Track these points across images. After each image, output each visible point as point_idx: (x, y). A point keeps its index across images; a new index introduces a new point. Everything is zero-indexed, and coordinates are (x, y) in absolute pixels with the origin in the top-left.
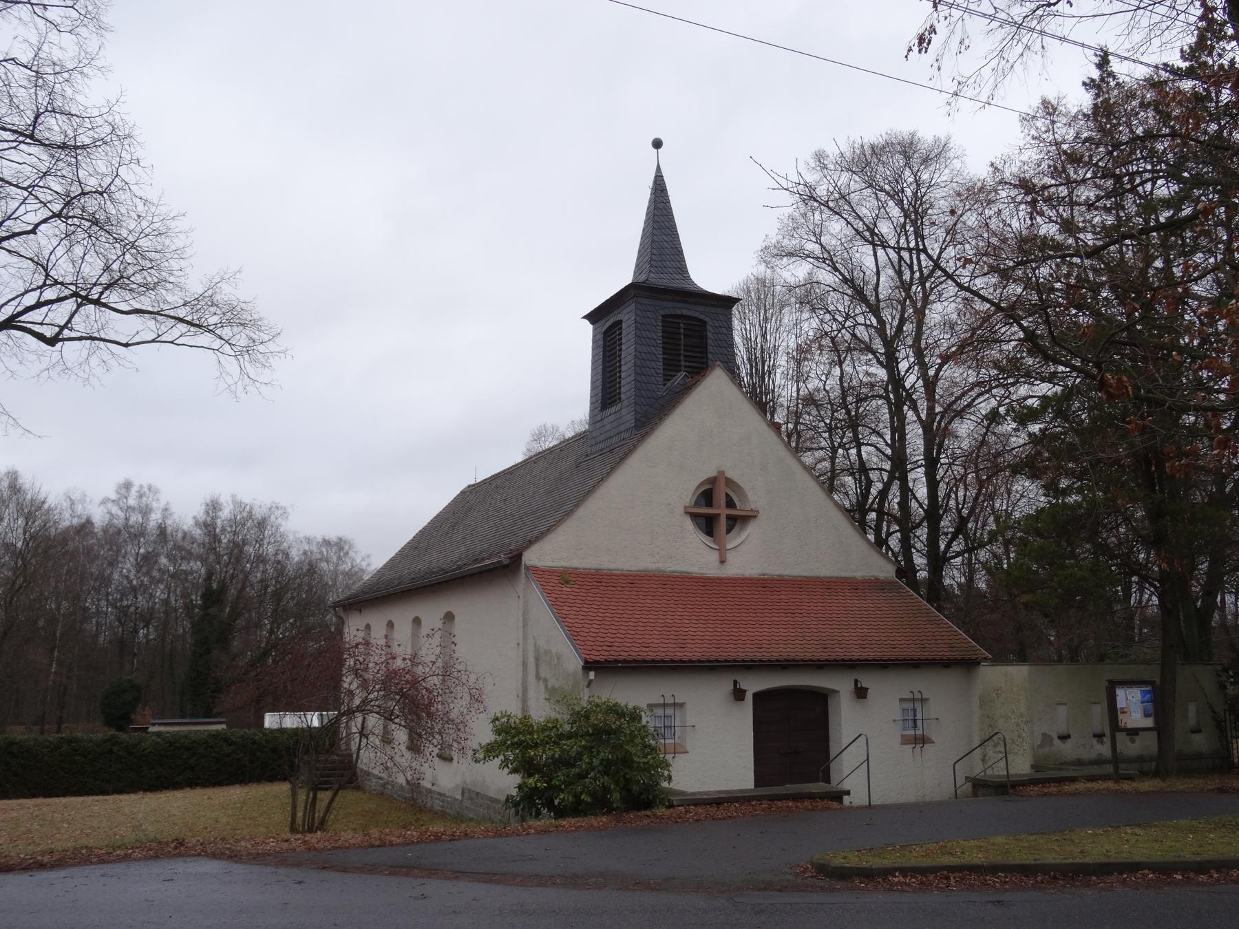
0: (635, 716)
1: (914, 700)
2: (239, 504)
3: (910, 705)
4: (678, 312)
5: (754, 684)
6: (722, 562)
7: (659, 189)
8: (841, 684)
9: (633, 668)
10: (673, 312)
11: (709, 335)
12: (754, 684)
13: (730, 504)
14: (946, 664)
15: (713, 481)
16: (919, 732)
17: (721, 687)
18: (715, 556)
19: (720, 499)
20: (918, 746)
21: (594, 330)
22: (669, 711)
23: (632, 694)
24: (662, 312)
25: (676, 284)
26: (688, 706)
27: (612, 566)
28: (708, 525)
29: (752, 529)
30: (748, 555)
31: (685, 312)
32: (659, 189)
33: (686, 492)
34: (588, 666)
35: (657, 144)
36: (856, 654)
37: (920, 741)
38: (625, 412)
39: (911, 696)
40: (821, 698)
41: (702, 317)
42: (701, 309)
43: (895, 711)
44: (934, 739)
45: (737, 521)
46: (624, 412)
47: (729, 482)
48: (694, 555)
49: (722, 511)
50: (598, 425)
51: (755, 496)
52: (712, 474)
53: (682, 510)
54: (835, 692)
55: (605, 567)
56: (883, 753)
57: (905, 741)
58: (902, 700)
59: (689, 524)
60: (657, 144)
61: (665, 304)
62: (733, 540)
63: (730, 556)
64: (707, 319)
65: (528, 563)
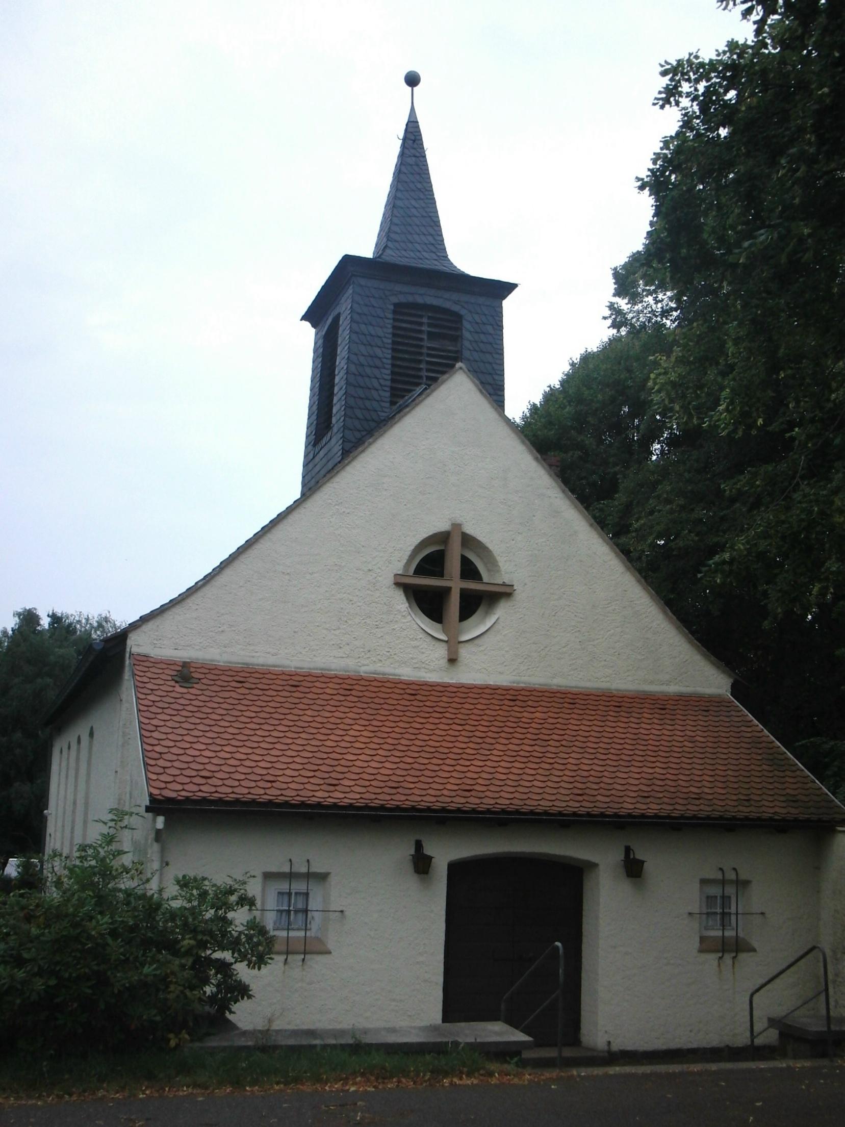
0: (223, 898)
1: (723, 882)
2: (56, 619)
3: (715, 891)
4: (420, 300)
5: (445, 852)
6: (452, 661)
7: (412, 139)
8: (603, 857)
9: (399, 817)
10: (410, 299)
11: (466, 334)
12: (445, 852)
13: (469, 571)
14: (778, 827)
15: (443, 538)
16: (729, 933)
17: (394, 853)
18: (441, 652)
19: (453, 565)
20: (728, 958)
21: (316, 334)
22: (299, 886)
23: (231, 863)
24: (395, 300)
25: (429, 263)
26: (333, 880)
27: (271, 660)
28: (429, 603)
29: (501, 611)
30: (494, 654)
31: (429, 300)
32: (412, 139)
33: (396, 553)
34: (156, 806)
35: (412, 80)
36: (629, 806)
37: (732, 948)
38: (334, 443)
39: (720, 877)
40: (572, 878)
41: (456, 308)
42: (455, 296)
43: (690, 898)
44: (755, 944)
45: (475, 602)
46: (333, 441)
47: (468, 541)
48: (410, 649)
49: (455, 583)
50: (311, 465)
51: (509, 563)
52: (443, 526)
53: (390, 580)
54: (593, 866)
55: (261, 661)
56: (648, 969)
57: (706, 946)
58: (704, 882)
59: (400, 602)
60: (412, 80)
61: (398, 288)
62: (474, 628)
63: (464, 653)
64: (463, 312)
65: (135, 650)
